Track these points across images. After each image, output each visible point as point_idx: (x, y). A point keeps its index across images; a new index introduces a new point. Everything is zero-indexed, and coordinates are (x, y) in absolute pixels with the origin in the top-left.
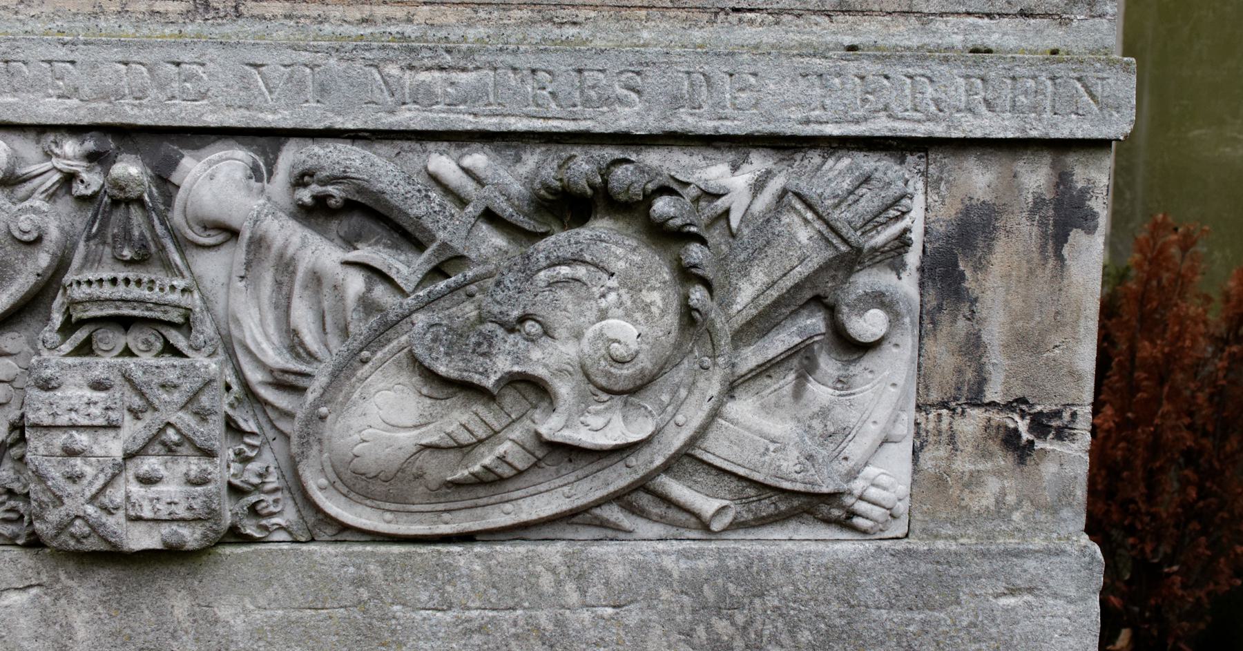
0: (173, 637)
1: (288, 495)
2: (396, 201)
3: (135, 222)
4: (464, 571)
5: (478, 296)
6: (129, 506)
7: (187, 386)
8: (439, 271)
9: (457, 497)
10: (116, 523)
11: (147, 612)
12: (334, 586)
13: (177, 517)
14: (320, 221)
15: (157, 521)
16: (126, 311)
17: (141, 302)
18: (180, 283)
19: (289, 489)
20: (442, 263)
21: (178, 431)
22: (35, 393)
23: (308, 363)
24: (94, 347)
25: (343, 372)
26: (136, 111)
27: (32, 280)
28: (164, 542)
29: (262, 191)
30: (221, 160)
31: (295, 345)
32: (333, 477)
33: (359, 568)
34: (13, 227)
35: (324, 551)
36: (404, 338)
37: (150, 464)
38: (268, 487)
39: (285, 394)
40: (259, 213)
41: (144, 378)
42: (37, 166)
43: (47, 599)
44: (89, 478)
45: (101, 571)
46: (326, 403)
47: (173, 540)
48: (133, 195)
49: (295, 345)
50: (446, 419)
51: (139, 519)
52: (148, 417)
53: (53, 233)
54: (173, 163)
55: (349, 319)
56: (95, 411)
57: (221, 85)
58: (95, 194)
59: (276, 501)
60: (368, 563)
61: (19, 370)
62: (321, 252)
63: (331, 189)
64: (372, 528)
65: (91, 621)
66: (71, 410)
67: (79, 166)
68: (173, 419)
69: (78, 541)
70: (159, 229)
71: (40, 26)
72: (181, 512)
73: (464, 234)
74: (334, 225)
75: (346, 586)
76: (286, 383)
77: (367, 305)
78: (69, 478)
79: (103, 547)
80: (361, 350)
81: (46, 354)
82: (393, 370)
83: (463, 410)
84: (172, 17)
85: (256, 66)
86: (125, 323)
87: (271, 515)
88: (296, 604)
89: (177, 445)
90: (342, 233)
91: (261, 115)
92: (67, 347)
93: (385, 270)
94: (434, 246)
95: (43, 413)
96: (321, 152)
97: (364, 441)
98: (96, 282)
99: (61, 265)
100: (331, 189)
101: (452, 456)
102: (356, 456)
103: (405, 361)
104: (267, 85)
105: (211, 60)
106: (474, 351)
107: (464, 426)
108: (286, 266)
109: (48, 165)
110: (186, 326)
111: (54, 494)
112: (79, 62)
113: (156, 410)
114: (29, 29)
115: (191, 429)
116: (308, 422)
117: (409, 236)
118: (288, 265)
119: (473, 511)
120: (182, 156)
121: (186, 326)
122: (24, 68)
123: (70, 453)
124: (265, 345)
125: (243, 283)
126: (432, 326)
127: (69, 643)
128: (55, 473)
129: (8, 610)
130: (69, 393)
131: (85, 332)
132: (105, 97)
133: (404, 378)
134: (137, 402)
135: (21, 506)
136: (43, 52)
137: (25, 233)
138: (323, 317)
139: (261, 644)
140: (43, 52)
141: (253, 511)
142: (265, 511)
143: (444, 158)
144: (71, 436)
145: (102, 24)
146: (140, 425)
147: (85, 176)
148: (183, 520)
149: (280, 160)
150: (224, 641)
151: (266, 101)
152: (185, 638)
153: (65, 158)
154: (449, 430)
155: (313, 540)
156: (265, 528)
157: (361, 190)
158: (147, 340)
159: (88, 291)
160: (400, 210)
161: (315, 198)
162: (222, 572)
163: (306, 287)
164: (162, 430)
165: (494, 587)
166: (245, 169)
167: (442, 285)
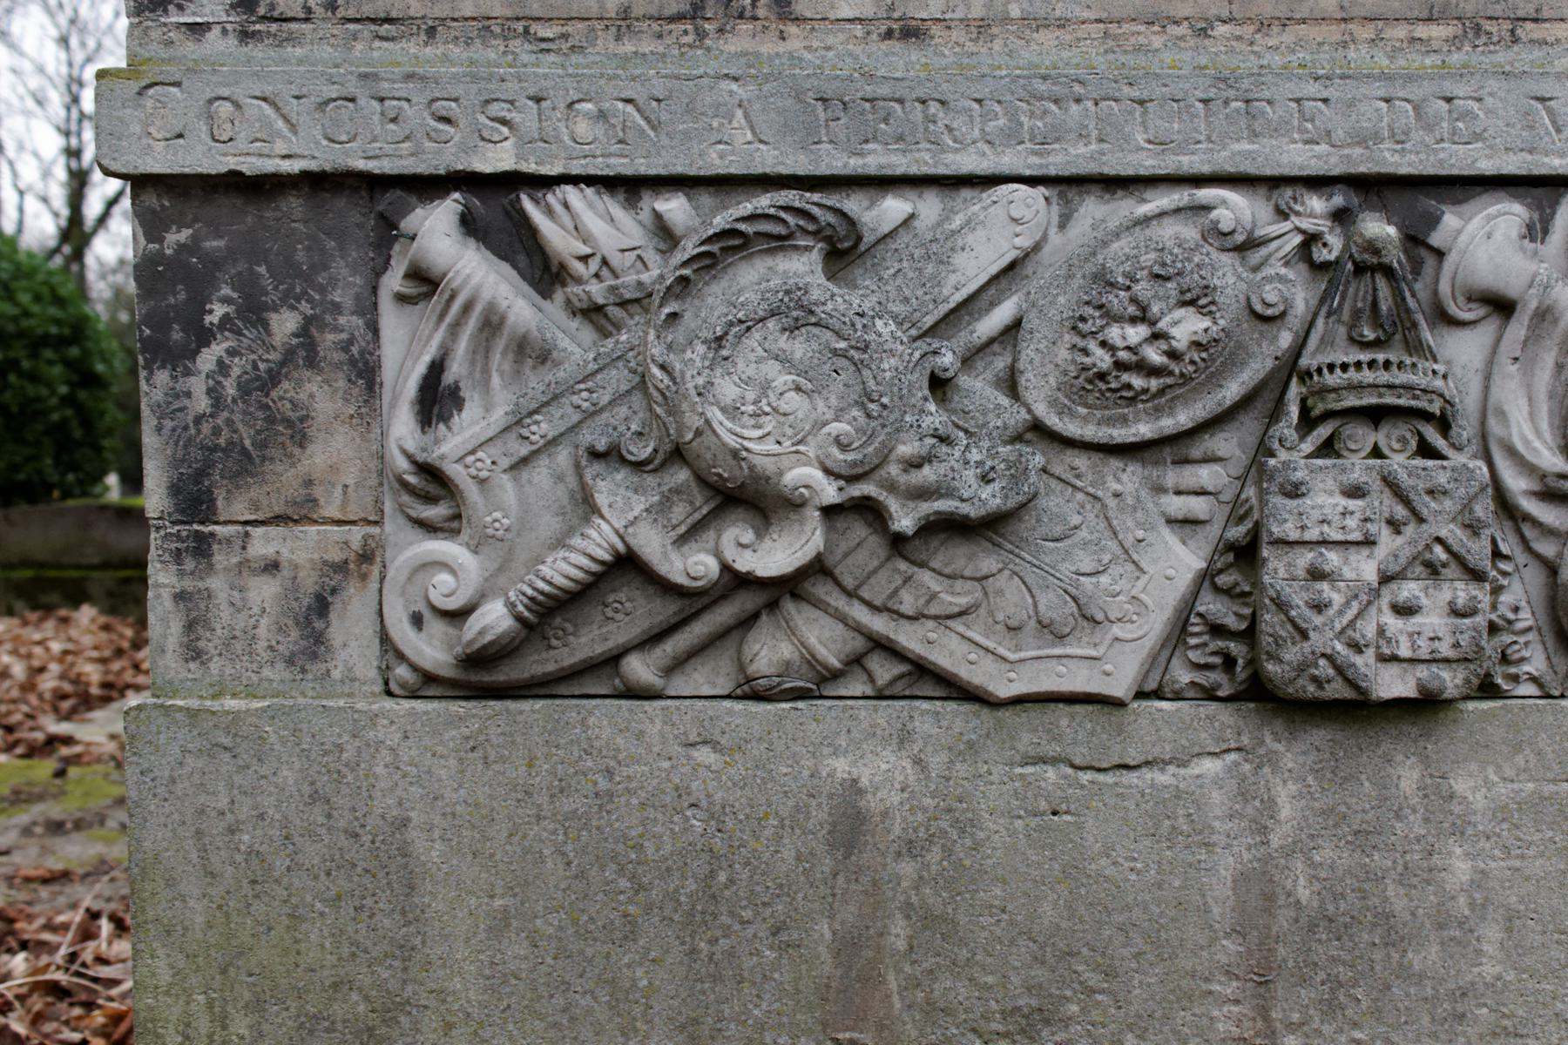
0: (1398, 817)
3: (1381, 294)
10: (1364, 663)
11: (1367, 784)
13: (1439, 656)
16: (1390, 399)
19: (1539, 629)
21: (1448, 549)
22: (1277, 500)
26: (1397, 157)
27: (1270, 364)
28: (1421, 687)
29: (1535, 253)
37: (1408, 590)
38: (1520, 625)
41: (1411, 482)
42: (1275, 227)
43: (1247, 767)
44: (1336, 607)
45: (1315, 731)
48: (1386, 260)
51: (1394, 658)
52: (1409, 530)
54: (1434, 221)
56: (1351, 522)
57: (1501, 123)
58: (1337, 261)
59: (1527, 644)
61: (1227, 479)
65: (1301, 795)
66: (1323, 521)
67: (1323, 225)
68: (1443, 533)
71: (1277, 60)
72: (1445, 650)
79: (1348, 694)
81: (1283, 455)
84: (1435, 45)
85: (1542, 100)
87: (1523, 660)
88: (1550, 776)
89: (1444, 565)
91: (1546, 160)
92: (1308, 446)
95: (1289, 525)
104: (1554, 122)
105: (1490, 94)
110: (1444, 424)
112: (1333, 100)
113: (1421, 520)
114: (1265, 62)
115: (1464, 546)
122: (1268, 109)
123: (1316, 574)
124: (1537, 444)
125: (1517, 366)
127: (1270, 823)
128: (1299, 599)
129: (1198, 782)
130: (1319, 501)
132: (1087, 260)
134: (1400, 512)
135: (1234, 647)
136: (1291, 88)
137: (1269, 305)
139: (1505, 826)
140: (1291, 88)
141: (1505, 659)
142: (1516, 656)
144: (1321, 554)
145: (1352, 55)
146: (1400, 540)
147: (1329, 238)
148: (1447, 661)
150: (1459, 822)
151: (1553, 142)
152: (1411, 818)
153: (1312, 215)
156: (1515, 679)
162: (1462, 733)
164: (1428, 547)
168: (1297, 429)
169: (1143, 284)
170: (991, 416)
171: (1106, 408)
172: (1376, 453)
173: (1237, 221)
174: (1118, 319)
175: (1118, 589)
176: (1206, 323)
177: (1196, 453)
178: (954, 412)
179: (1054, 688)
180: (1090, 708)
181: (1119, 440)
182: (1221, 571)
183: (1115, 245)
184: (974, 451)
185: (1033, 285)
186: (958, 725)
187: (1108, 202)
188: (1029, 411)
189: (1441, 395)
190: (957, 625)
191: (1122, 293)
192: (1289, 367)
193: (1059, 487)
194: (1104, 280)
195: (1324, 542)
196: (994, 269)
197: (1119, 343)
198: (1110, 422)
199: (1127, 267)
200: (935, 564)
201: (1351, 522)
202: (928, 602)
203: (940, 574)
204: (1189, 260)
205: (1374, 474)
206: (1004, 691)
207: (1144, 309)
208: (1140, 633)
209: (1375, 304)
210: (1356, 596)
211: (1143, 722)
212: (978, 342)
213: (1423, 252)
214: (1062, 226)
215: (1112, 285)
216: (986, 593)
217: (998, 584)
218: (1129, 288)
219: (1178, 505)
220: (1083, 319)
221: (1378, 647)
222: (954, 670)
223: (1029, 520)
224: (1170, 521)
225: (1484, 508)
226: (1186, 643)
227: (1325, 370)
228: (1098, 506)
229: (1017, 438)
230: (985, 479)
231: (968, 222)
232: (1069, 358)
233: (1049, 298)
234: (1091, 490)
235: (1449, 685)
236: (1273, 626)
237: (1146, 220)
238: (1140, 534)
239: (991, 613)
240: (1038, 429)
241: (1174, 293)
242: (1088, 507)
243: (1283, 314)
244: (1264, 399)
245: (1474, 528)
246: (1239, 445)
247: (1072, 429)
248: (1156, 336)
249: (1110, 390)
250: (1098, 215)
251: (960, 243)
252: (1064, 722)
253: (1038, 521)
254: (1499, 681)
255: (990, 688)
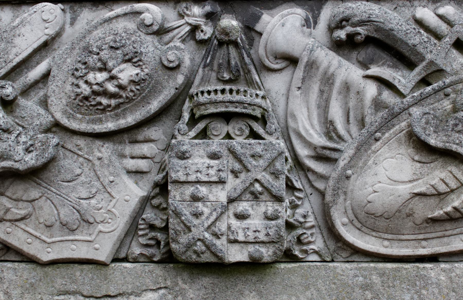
1: (319, 231)
2: (401, 35)
3: (232, 56)
4: (434, 280)
5: (452, 95)
6: (230, 233)
7: (268, 156)
8: (425, 82)
9: (432, 229)
10: (221, 243)
12: (349, 290)
13: (259, 240)
14: (346, 52)
15: (246, 243)
16: (231, 109)
17: (241, 103)
18: (261, 93)
19: (319, 227)
20: (428, 75)
21: (262, 185)
22: (175, 161)
23: (338, 143)
24: (208, 133)
25: (363, 147)
27: (173, 91)
28: (251, 256)
29: (310, 34)
30: (289, 14)
31: (329, 130)
32: (352, 217)
33: (365, 278)
34: (163, 59)
35: (343, 268)
36: (403, 124)
37: (243, 206)
38: (308, 225)
39: (322, 164)
40: (313, 46)
41: (242, 151)
42: (176, 22)
44: (206, 215)
45: (203, 279)
46: (351, 168)
47: (257, 255)
48: (233, 38)
49: (329, 130)
50: (431, 176)
51: (236, 241)
52: (243, 176)
53: (187, 62)
54: (257, 18)
55: (366, 113)
56: (212, 172)
58: (209, 39)
59: (312, 235)
60: (372, 274)
61: (157, 151)
62: (348, 71)
63: (359, 29)
64: (376, 251)
66: (197, 171)
67: (201, 21)
68: (259, 177)
69: (198, 256)
70: (247, 60)
72: (262, 237)
73: (443, 55)
74: (354, 55)
75: (357, 289)
76: (321, 157)
77: (378, 104)
78: (194, 215)
79: (213, 259)
80: (376, 132)
81: (180, 138)
82: (395, 145)
83: (442, 170)
86: (227, 117)
87: (309, 243)
89: (261, 194)
90: (361, 59)
92: (192, 133)
93: (391, 80)
94: (424, 63)
95: (180, 173)
96: (354, 6)
97: (375, 192)
98: (211, 92)
99: (188, 84)
100: (359, 29)
101: (432, 201)
102: (369, 202)
103: (403, 139)
106: (453, 130)
107: (443, 180)
108: (328, 80)
109: (182, 22)
110: (263, 121)
111: (185, 225)
113: (248, 171)
115: (270, 183)
116: (339, 180)
117: (404, 58)
118: (329, 79)
119: (442, 239)
120: (262, 14)
121: (263, 121)
123: (195, 198)
124: (312, 131)
125: (300, 92)
126: (425, 114)
128: (186, 211)
130: (196, 161)
131: (203, 122)
132: (81, 40)
133: (403, 150)
134: (237, 166)
135: (160, 236)
137: (171, 62)
138: (348, 113)
141: (299, 241)
142: (306, 241)
143: (426, 9)
144: (197, 188)
146: (238, 181)
147: (204, 28)
148: (263, 242)
149: (322, 15)
153: (194, 16)
154: (433, 183)
155: (333, 261)
156: (306, 252)
157: (378, 30)
158: (241, 128)
159: (209, 97)
160: (402, 41)
161: (348, 35)
162: (279, 280)
163: (340, 93)
164: (252, 184)
165: (454, 291)
166: (302, 20)
167: (429, 89)
168: (187, 124)
169: (105, 52)
170: (35, 119)
171: (91, 114)
172: (228, 136)
173: (154, 19)
174: (93, 69)
175: (100, 206)
176: (138, 71)
177: (140, 137)
178: (17, 117)
179: (70, 256)
180: (91, 266)
181: (98, 131)
182: (153, 197)
183: (95, 33)
184: (23, 136)
185: (56, 54)
186: (26, 275)
187: (95, 11)
188: (53, 117)
189: (260, 107)
190: (21, 225)
191: (95, 56)
192: (183, 93)
193: (71, 155)
194: (88, 50)
195: (198, 182)
196: (35, 46)
197: (93, 81)
198: (94, 122)
199: (99, 43)
200: (8, 194)
201: (212, 172)
202: (6, 213)
203: (11, 198)
204: (129, 39)
205: (224, 147)
206: (45, 258)
207: (105, 64)
208: (112, 228)
209: (229, 62)
210: (215, 210)
211: (117, 274)
212: (30, 82)
213: (254, 34)
214: (72, 24)
215: (90, 52)
216: (34, 209)
217: (40, 204)
218: (98, 54)
219: (132, 164)
220: (77, 70)
221: (228, 236)
222: (21, 247)
223: (53, 170)
224: (129, 172)
225: (283, 167)
226: (138, 234)
227: (200, 95)
228: (90, 164)
229: (47, 131)
230: (28, 151)
231: (22, 22)
232: (71, 89)
233: (63, 60)
234: (86, 156)
235: (265, 255)
236: (174, 225)
237: (110, 20)
238: (111, 178)
239: (37, 219)
240: (56, 127)
241: (120, 56)
242: (85, 165)
243: (178, 66)
244: (169, 110)
245: (276, 175)
246: (164, 134)
247: (74, 125)
248: (112, 78)
249: (91, 105)
250: (90, 18)
251: (18, 32)
252: (78, 273)
253: (59, 172)
254: (297, 253)
255: (39, 256)
